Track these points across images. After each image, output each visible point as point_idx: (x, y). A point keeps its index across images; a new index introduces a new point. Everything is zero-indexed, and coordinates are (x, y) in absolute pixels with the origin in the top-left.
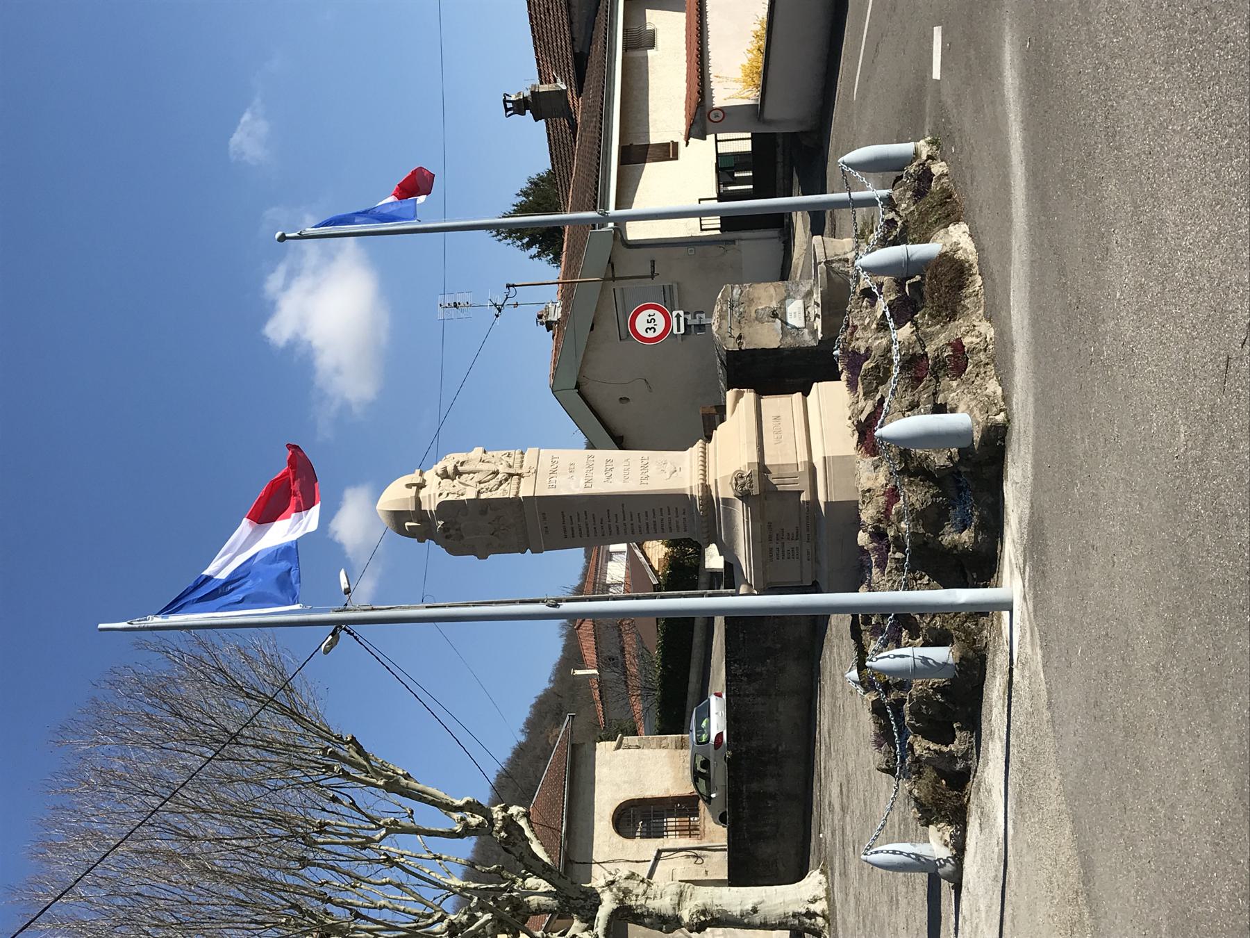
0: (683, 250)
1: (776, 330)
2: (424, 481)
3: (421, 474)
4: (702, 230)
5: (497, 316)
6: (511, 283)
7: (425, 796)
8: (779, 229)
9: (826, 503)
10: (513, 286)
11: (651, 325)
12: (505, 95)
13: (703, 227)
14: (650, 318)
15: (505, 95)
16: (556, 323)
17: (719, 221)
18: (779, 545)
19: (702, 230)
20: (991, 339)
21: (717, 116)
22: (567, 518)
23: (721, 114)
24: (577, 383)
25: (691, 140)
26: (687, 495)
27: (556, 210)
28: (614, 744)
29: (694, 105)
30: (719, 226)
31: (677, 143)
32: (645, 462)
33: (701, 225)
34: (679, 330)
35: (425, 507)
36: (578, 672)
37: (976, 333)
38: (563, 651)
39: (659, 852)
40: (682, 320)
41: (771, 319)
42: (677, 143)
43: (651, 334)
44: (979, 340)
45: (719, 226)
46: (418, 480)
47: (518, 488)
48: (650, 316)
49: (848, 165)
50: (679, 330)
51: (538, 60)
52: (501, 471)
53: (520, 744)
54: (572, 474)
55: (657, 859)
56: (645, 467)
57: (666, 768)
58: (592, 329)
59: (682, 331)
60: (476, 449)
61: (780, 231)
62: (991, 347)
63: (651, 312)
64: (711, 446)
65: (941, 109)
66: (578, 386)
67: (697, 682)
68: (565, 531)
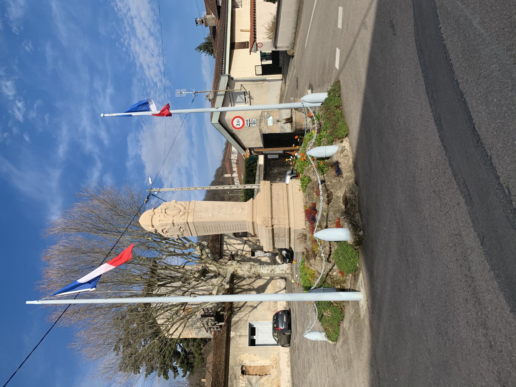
0: (251, 83)
1: (279, 127)
5: (192, 102)
6: (196, 92)
11: (238, 123)
12: (196, 19)
14: (238, 121)
15: (196, 19)
17: (261, 68)
18: (278, 239)
20: (357, 195)
27: (202, 107)
28: (248, 50)
34: (247, 125)
40: (248, 121)
41: (277, 123)
43: (238, 127)
44: (353, 195)
47: (187, 218)
50: (247, 125)
51: (206, 6)
62: (357, 199)
64: (255, 200)
66: (219, 121)
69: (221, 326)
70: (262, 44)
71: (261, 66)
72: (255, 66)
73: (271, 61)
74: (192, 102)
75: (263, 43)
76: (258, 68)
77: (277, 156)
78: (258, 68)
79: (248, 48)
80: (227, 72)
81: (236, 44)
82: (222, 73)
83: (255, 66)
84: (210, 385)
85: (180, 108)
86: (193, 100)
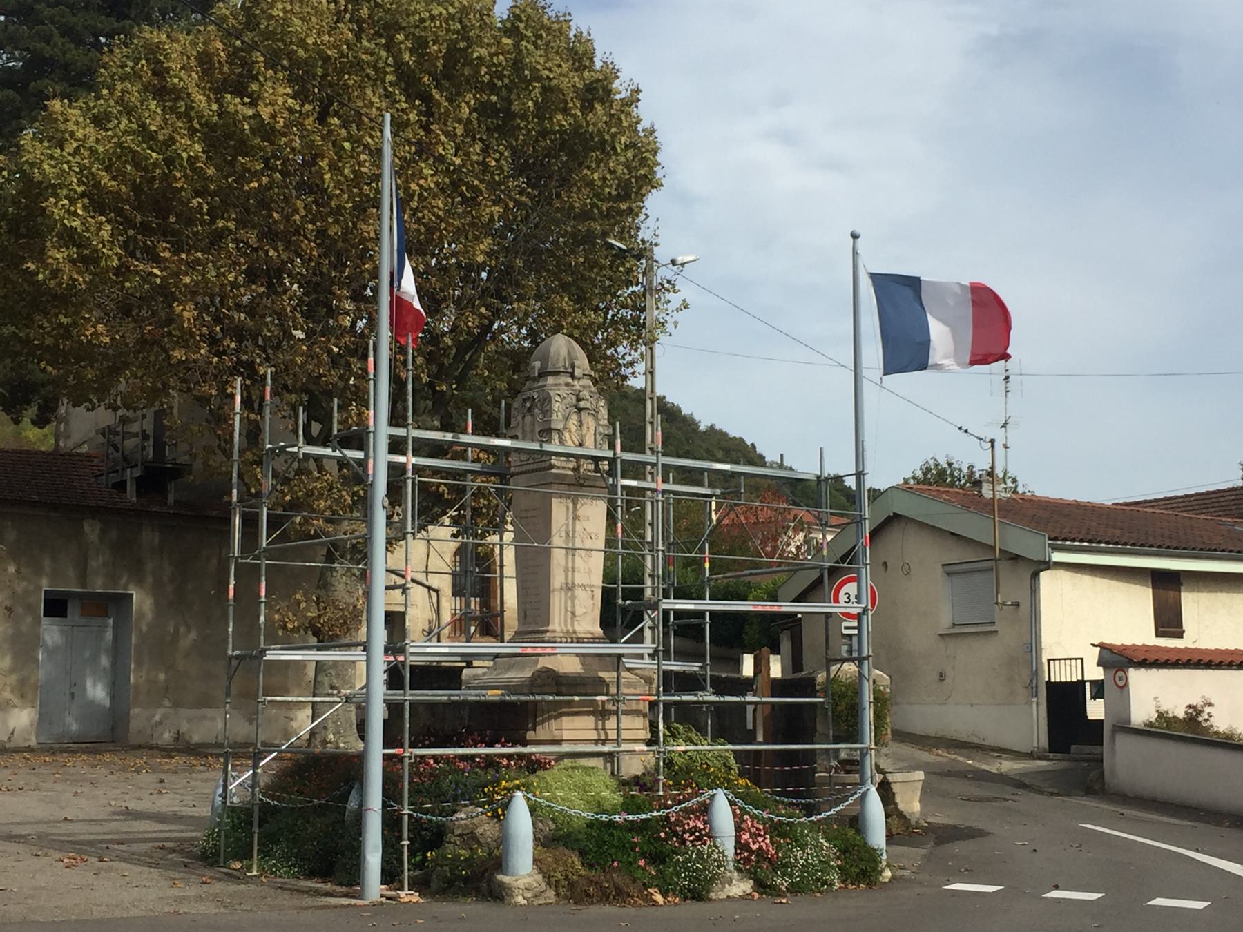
4: (1049, 661)
5: (960, 428)
7: (371, 353)
8: (1047, 747)
10: (993, 446)
13: (1052, 662)
16: (980, 492)
19: (1049, 661)
21: (1120, 679)
23: (1121, 683)
25: (1098, 649)
26: (548, 625)
29: (1129, 653)
30: (1053, 680)
31: (1182, 637)
33: (1054, 660)
34: (846, 628)
35: (551, 380)
39: (437, 591)
42: (1182, 637)
45: (1053, 680)
46: (578, 372)
49: (864, 795)
50: (846, 628)
53: (696, 424)
55: (429, 588)
59: (845, 632)
61: (1044, 749)
66: (896, 516)
69: (121, 486)
70: (1122, 687)
71: (1080, 678)
72: (1082, 659)
73: (1090, 718)
74: (960, 428)
75: (1125, 689)
76: (1074, 669)
77: (750, 726)
78: (1074, 669)
79: (1158, 634)
80: (1058, 557)
81: (1171, 594)
82: (1056, 539)
83: (1082, 659)
84: (351, 726)
85: (435, 685)
86: (966, 431)
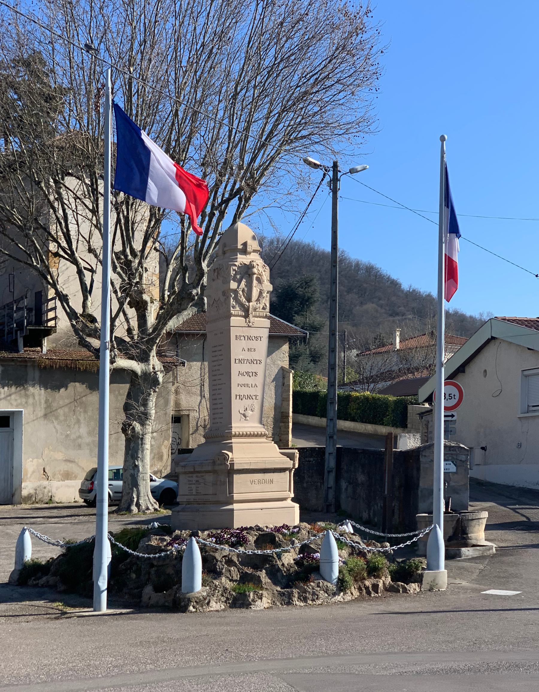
2: (250, 253)
3: (255, 251)
9: (232, 510)
14: (452, 395)
18: (194, 482)
22: (219, 348)
24: (497, 338)
32: (254, 397)
36: (398, 333)
37: (256, 599)
38: (471, 317)
48: (454, 395)
52: (251, 304)
54: (246, 350)
56: (249, 397)
57: (268, 405)
58: (529, 349)
60: (272, 286)
63: (457, 397)
65: (476, 590)
66: (493, 338)
67: (345, 427)
68: (220, 346)
